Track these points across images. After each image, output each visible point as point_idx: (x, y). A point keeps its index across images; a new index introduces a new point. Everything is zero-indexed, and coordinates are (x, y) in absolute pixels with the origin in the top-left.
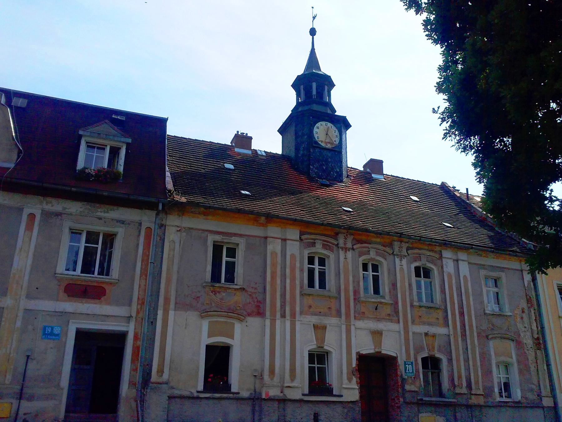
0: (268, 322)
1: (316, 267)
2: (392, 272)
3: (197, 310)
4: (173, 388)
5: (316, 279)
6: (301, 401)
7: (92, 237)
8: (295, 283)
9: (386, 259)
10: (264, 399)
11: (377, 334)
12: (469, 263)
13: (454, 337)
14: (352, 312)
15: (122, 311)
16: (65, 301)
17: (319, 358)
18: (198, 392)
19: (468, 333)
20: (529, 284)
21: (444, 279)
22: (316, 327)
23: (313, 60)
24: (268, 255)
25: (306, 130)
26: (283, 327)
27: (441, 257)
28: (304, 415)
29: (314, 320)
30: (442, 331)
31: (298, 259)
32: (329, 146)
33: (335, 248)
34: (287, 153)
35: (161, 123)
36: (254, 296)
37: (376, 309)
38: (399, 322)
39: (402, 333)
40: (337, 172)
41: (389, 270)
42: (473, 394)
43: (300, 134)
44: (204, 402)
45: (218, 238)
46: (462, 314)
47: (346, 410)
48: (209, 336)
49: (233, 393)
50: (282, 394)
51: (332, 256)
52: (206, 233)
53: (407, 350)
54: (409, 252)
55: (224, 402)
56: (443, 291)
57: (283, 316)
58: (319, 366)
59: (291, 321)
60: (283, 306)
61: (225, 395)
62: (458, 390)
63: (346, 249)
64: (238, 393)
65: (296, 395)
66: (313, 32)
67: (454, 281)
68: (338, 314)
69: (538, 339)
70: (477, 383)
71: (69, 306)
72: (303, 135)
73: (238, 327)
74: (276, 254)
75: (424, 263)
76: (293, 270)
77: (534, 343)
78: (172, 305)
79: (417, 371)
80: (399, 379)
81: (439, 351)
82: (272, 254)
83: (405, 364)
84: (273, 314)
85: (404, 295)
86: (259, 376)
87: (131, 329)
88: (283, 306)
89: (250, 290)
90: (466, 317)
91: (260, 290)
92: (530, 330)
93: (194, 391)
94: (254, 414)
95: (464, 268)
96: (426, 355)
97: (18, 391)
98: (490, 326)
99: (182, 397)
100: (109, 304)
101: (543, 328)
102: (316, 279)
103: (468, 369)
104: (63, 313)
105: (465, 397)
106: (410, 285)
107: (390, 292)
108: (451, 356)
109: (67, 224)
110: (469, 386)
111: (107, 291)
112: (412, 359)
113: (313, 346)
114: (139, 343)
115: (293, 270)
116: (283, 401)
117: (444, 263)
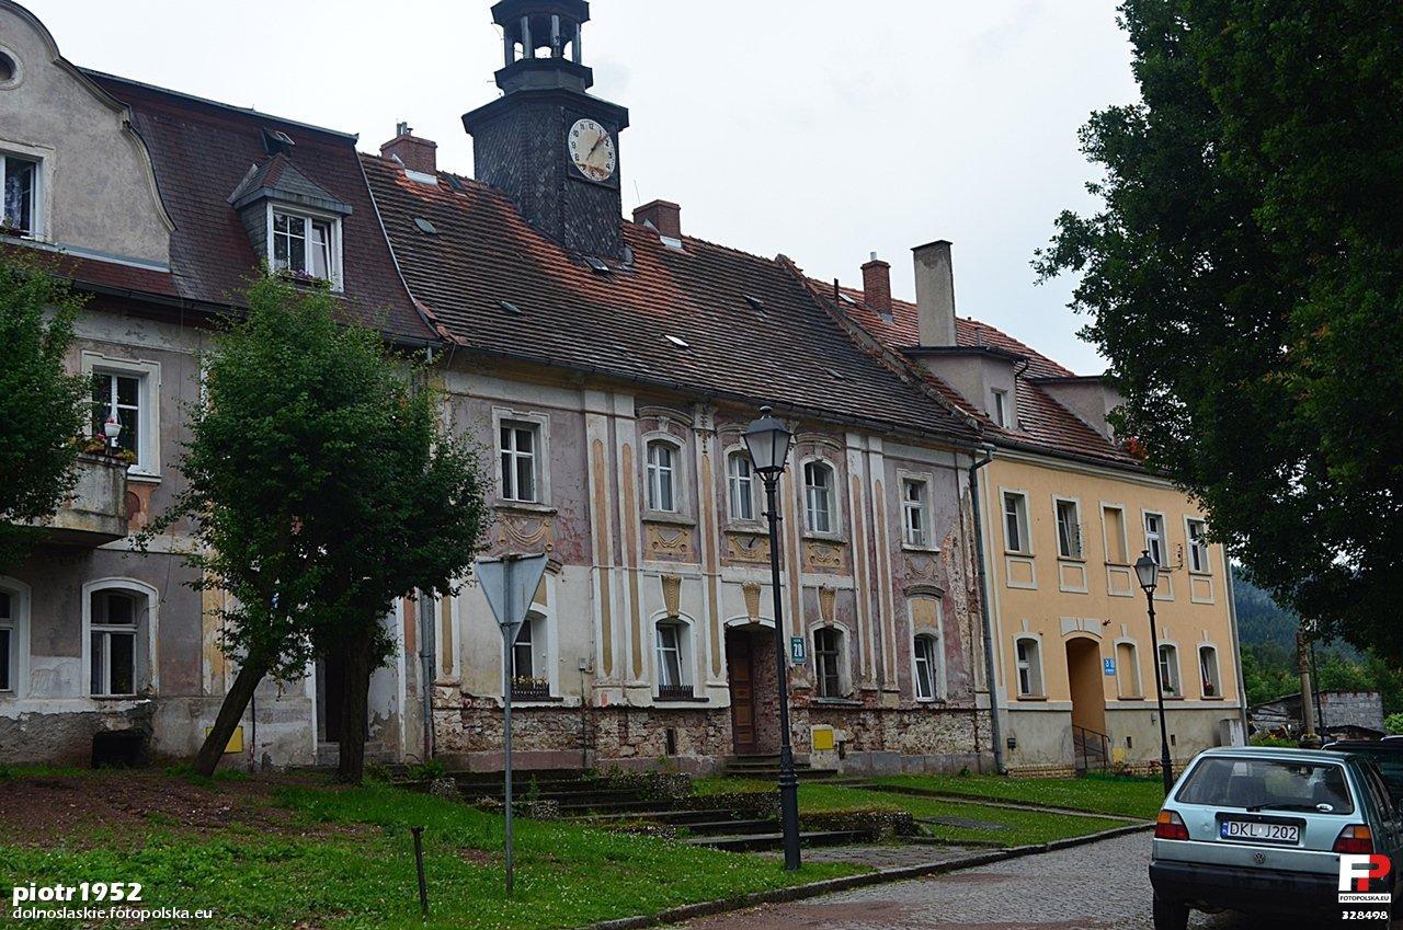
0: (596, 573)
6: (650, 709)
12: (884, 457)
20: (966, 493)
25: (550, 138)
26: (618, 580)
27: (845, 448)
30: (846, 582)
32: (597, 178)
33: (688, 431)
35: (351, 141)
45: (507, 413)
46: (872, 551)
49: (554, 700)
51: (683, 447)
52: (488, 403)
57: (618, 562)
64: (561, 700)
65: (645, 700)
68: (697, 558)
70: (891, 671)
75: (819, 458)
81: (840, 618)
84: (603, 560)
92: (963, 577)
95: (877, 462)
96: (821, 626)
101: (982, 573)
110: (880, 680)
112: (803, 634)
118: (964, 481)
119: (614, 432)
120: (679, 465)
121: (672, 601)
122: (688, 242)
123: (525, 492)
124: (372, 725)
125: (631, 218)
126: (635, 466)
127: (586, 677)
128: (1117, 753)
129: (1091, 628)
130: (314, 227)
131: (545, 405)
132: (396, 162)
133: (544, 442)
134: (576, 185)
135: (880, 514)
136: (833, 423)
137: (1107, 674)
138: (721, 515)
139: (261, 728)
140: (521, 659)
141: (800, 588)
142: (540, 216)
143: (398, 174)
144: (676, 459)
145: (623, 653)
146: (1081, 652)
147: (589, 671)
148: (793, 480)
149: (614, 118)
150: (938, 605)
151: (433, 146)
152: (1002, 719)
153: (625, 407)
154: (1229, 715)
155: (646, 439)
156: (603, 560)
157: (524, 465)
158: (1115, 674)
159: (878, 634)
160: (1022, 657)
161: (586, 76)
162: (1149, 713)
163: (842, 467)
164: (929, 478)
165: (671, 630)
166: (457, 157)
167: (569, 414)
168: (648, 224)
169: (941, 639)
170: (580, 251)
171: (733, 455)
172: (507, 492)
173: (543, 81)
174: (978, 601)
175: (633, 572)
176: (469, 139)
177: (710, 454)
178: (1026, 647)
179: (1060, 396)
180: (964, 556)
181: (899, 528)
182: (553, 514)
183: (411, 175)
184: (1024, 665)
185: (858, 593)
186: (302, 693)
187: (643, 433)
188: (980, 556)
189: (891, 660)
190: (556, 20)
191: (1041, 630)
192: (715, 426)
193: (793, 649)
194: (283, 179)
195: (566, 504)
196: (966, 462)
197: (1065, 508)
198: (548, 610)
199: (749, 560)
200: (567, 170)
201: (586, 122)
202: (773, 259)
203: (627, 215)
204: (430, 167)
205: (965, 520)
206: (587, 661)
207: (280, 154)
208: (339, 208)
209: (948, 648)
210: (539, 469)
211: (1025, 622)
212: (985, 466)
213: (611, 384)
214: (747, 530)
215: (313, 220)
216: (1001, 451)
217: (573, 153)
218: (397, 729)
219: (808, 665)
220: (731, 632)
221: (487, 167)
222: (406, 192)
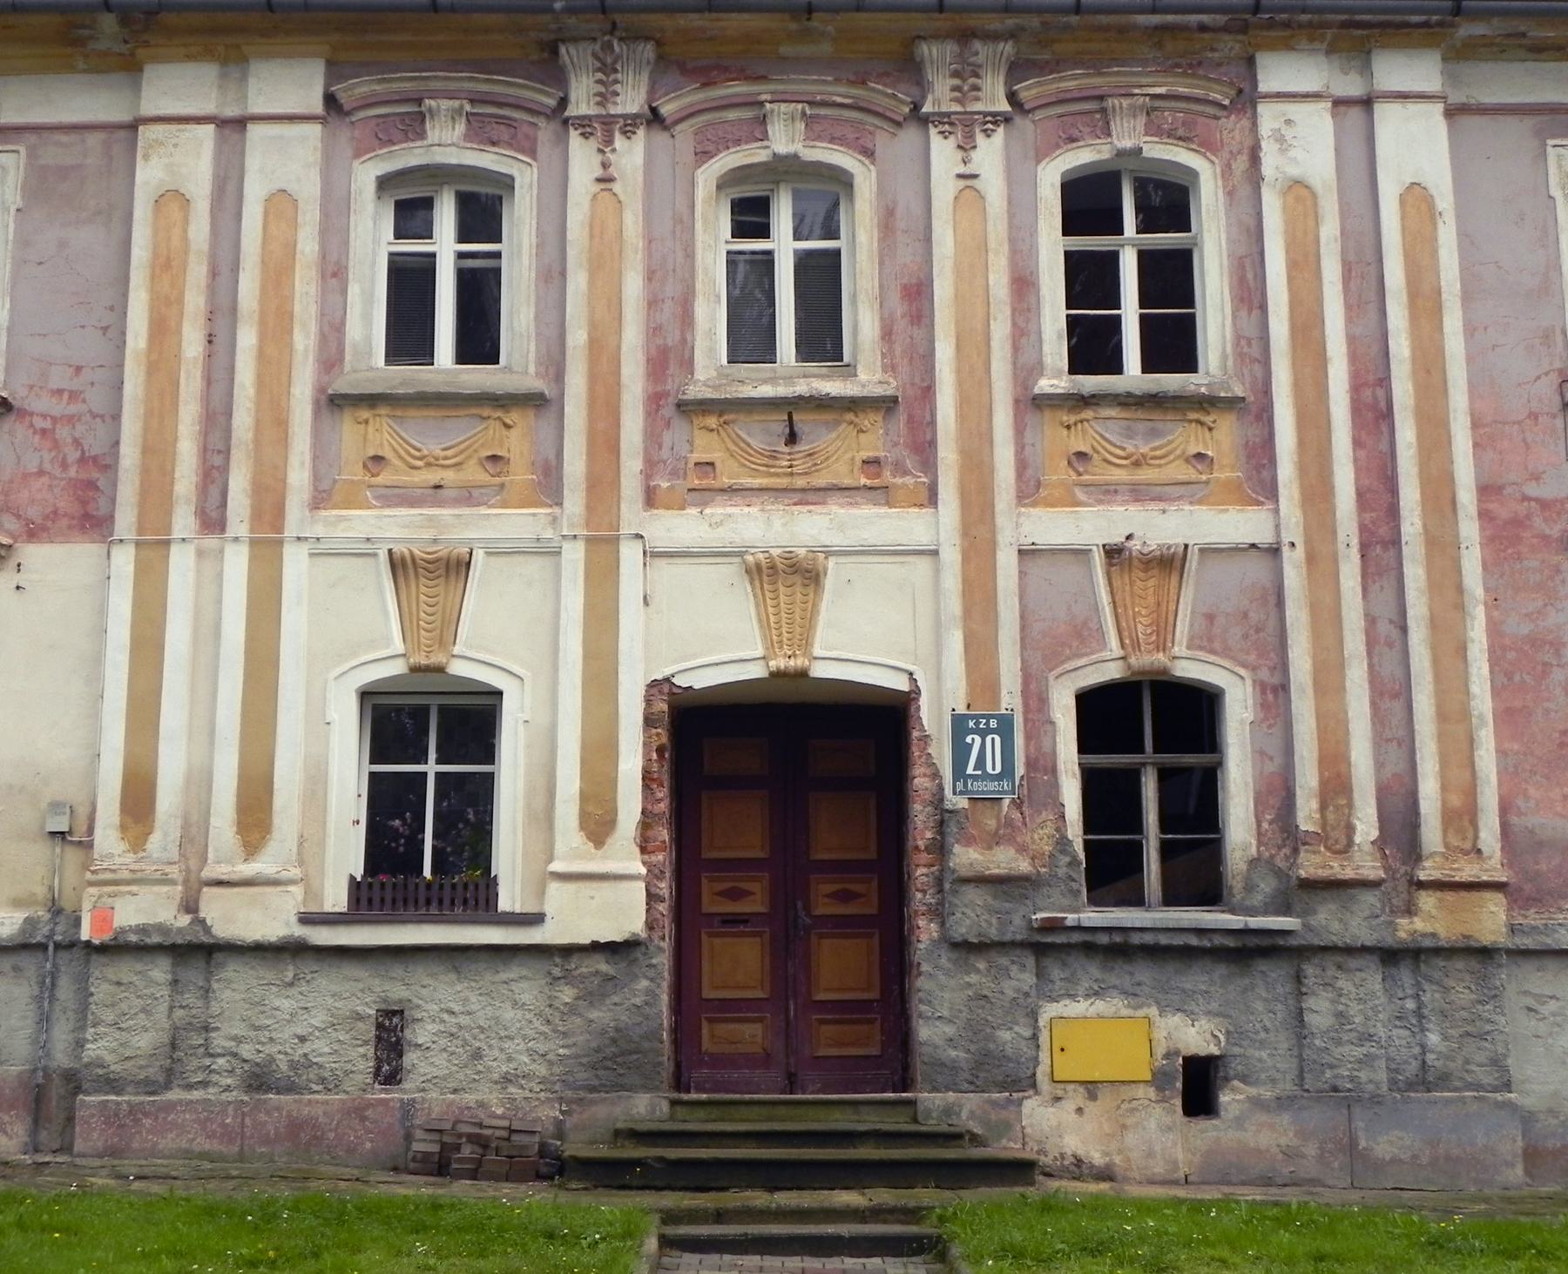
0: (124, 560)
1: (445, 244)
2: (907, 228)
5: (446, 310)
8: (290, 346)
9: (869, 153)
11: (789, 579)
12: (1453, 112)
13: (1311, 559)
14: (632, 466)
17: (431, 740)
21: (1259, 215)
24: (139, 213)
26: (207, 586)
27: (1246, 99)
28: (319, 1018)
29: (401, 527)
30: (1240, 525)
31: (310, 218)
36: (63, 433)
37: (792, 438)
38: (932, 499)
39: (951, 556)
42: (1422, 885)
46: (1374, 415)
47: (567, 994)
50: (184, 920)
51: (526, 178)
53: (980, 652)
54: (1029, 90)
57: (213, 521)
58: (432, 755)
59: (254, 543)
60: (213, 474)
62: (1311, 865)
65: (269, 919)
67: (1330, 230)
70: (1462, 816)
74: (185, 202)
75: (1127, 143)
76: (277, 275)
79: (1043, 766)
81: (1205, 641)
82: (158, 202)
85: (973, 346)
88: (213, 474)
89: (42, 404)
90: (1406, 434)
94: (44, 1021)
96: (1112, 672)
102: (446, 310)
103: (1395, 732)
105: (1370, 899)
106: (1024, 284)
107: (887, 334)
108: (1283, 666)
112: (1010, 699)
116: (198, 953)
127: (73, 856)
135: (1425, 304)
136: (1184, 28)
141: (1007, 561)
145: (200, 782)
147: (70, 837)
148: (997, 230)
159: (1391, 693)
167: (94, 140)
187: (357, 155)
195: (59, 378)
199: (783, 482)
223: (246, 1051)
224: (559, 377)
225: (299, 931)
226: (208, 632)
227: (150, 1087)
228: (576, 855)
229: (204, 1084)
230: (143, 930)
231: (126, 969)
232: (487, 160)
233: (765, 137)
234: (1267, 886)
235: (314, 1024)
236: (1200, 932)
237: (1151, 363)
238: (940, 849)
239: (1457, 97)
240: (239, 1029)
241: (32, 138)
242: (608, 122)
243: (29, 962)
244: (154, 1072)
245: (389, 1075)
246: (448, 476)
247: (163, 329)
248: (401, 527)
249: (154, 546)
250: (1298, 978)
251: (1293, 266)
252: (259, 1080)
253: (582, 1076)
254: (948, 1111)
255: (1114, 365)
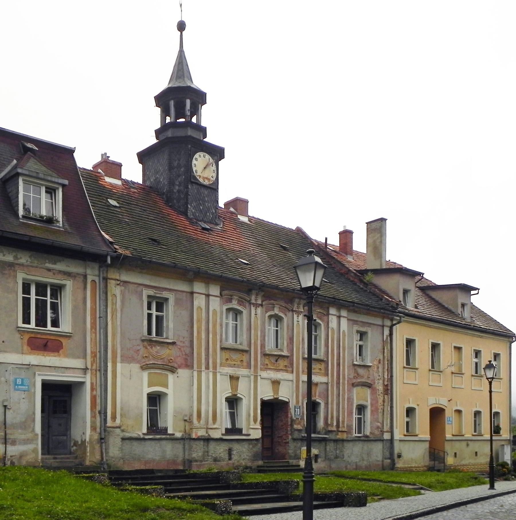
0: (195, 374)
3: (138, 362)
4: (123, 431)
6: (221, 440)
7: (41, 289)
9: (286, 315)
10: (194, 439)
11: (276, 383)
12: (348, 320)
15: (78, 363)
16: (30, 353)
18: (144, 434)
19: (341, 381)
20: (387, 338)
22: (232, 378)
23: (181, 67)
24: (195, 310)
25: (183, 162)
26: (207, 377)
27: (328, 314)
28: (222, 450)
29: (230, 371)
32: (206, 183)
33: (247, 304)
34: (148, 183)
35: (70, 152)
36: (182, 349)
39: (295, 381)
40: (213, 214)
41: (288, 326)
42: (340, 431)
43: (176, 164)
44: (148, 443)
45: (151, 292)
46: (339, 365)
47: (251, 446)
48: (149, 386)
49: (170, 435)
51: (245, 312)
52: (141, 287)
55: (164, 442)
56: (327, 345)
57: (207, 368)
59: (213, 372)
61: (164, 436)
62: (330, 428)
63: (256, 306)
64: (174, 434)
65: (216, 434)
66: (181, 26)
68: (249, 367)
69: (387, 385)
70: (343, 422)
71: (34, 359)
72: (179, 166)
73: (171, 378)
76: (214, 326)
77: (384, 389)
78: (119, 359)
80: (289, 420)
83: (295, 408)
84: (199, 366)
85: (298, 349)
86: (188, 421)
87: (88, 380)
90: (341, 368)
91: (187, 343)
92: (382, 378)
93: (140, 434)
94: (184, 451)
95: (344, 323)
97: (4, 437)
98: (356, 375)
99: (131, 439)
100: (66, 356)
101: (392, 376)
104: (29, 366)
105: (334, 433)
106: (303, 339)
107: (287, 345)
109: (21, 277)
110: (338, 426)
111: (64, 344)
112: (300, 404)
113: (228, 393)
114: (94, 393)
115: (214, 326)
116: (207, 440)
117: (330, 319)
118: (387, 332)
119: (209, 303)
120: (242, 320)
121: (235, 387)
122: (251, 219)
123: (159, 333)
124: (72, 447)
125: (223, 207)
126: (218, 320)
127: (187, 424)
128: (450, 460)
129: (443, 402)
130: (46, 192)
131: (172, 287)
132: (99, 173)
133: (170, 309)
134: (195, 186)
136: (323, 302)
137: (448, 424)
138: (263, 346)
139: (10, 448)
140: (153, 416)
142: (175, 201)
143: (101, 179)
144: (240, 318)
145: (207, 412)
146: (437, 414)
149: (217, 153)
150: (368, 391)
151: (120, 165)
152: (396, 445)
153: (215, 290)
154: (503, 443)
155: (225, 308)
156: (199, 366)
157: (159, 319)
158: (452, 423)
160: (407, 416)
161: (203, 131)
162: (466, 442)
163: (326, 324)
164: (369, 330)
165: (233, 402)
166: (133, 172)
167: (185, 294)
168: (232, 209)
169: (369, 407)
170: (195, 219)
171: (270, 317)
172: (150, 332)
173: (180, 133)
174: (388, 390)
175: (215, 374)
176: (141, 166)
177: (259, 316)
178: (410, 412)
179: (434, 294)
180: (384, 368)
181: (352, 354)
182: (174, 343)
183: (108, 180)
184: (408, 419)
185: (330, 385)
186: (33, 431)
187: (224, 304)
188: (392, 368)
189: (344, 417)
190: (188, 102)
191: (418, 403)
192: (262, 302)
193: (295, 411)
194: (29, 164)
196: (388, 323)
197: (435, 347)
198: (170, 391)
200: (191, 178)
201: (202, 154)
202: (294, 229)
203: (221, 204)
204: (118, 176)
205: (386, 351)
206: (188, 416)
207: (29, 153)
208: (61, 181)
209: (372, 412)
210: (168, 321)
211: (411, 399)
212: (397, 325)
213: (208, 278)
214: (276, 353)
215: (46, 188)
216: (406, 318)
217: (194, 169)
218: (85, 448)
219: (302, 418)
220: (265, 404)
221: (149, 179)
222: (105, 187)
223: (214, 455)
224: (250, 347)
225: (222, 437)
226: (208, 387)
227: (201, 461)
228: (253, 425)
229: (207, 461)
230: (201, 436)
231: (197, 443)
232: (239, 308)
233: (274, 310)
234: (324, 431)
235: (220, 450)
236: (319, 437)
237: (53, 326)
238: (292, 425)
239: (349, 318)
240: (212, 452)
241: (175, 292)
242: (257, 304)
243: (182, 442)
244: (202, 459)
245: (230, 459)
246: (236, 363)
247: (199, 333)
248: (230, 371)
249: (200, 372)
250: (326, 444)
251: (331, 341)
252: (215, 460)
253: (253, 458)
254: (292, 463)
255: (45, 326)
